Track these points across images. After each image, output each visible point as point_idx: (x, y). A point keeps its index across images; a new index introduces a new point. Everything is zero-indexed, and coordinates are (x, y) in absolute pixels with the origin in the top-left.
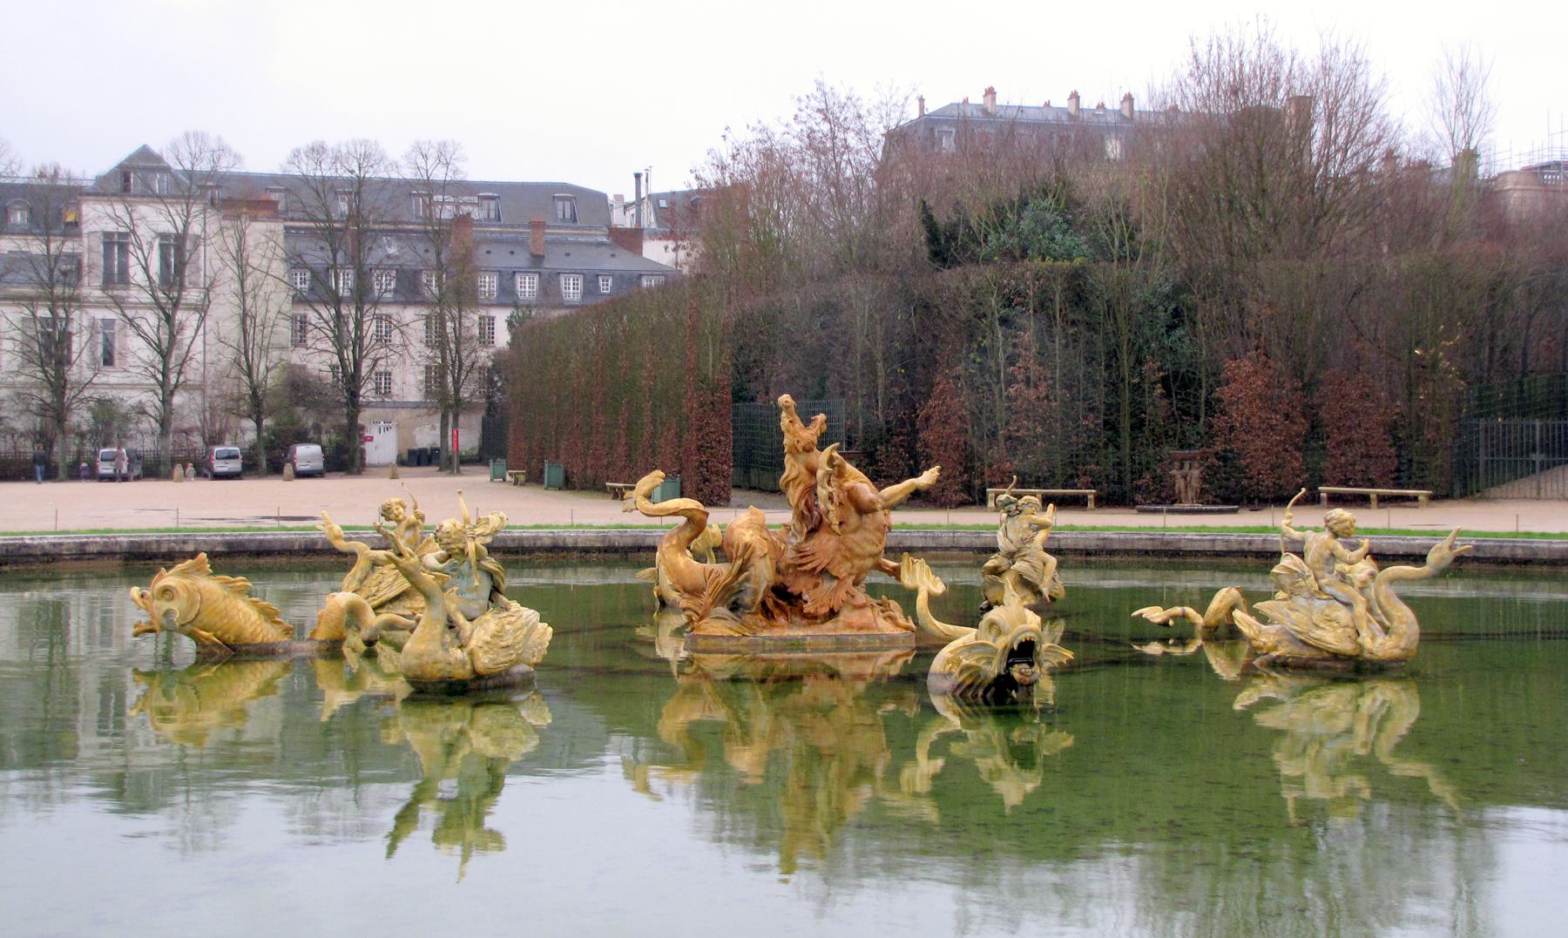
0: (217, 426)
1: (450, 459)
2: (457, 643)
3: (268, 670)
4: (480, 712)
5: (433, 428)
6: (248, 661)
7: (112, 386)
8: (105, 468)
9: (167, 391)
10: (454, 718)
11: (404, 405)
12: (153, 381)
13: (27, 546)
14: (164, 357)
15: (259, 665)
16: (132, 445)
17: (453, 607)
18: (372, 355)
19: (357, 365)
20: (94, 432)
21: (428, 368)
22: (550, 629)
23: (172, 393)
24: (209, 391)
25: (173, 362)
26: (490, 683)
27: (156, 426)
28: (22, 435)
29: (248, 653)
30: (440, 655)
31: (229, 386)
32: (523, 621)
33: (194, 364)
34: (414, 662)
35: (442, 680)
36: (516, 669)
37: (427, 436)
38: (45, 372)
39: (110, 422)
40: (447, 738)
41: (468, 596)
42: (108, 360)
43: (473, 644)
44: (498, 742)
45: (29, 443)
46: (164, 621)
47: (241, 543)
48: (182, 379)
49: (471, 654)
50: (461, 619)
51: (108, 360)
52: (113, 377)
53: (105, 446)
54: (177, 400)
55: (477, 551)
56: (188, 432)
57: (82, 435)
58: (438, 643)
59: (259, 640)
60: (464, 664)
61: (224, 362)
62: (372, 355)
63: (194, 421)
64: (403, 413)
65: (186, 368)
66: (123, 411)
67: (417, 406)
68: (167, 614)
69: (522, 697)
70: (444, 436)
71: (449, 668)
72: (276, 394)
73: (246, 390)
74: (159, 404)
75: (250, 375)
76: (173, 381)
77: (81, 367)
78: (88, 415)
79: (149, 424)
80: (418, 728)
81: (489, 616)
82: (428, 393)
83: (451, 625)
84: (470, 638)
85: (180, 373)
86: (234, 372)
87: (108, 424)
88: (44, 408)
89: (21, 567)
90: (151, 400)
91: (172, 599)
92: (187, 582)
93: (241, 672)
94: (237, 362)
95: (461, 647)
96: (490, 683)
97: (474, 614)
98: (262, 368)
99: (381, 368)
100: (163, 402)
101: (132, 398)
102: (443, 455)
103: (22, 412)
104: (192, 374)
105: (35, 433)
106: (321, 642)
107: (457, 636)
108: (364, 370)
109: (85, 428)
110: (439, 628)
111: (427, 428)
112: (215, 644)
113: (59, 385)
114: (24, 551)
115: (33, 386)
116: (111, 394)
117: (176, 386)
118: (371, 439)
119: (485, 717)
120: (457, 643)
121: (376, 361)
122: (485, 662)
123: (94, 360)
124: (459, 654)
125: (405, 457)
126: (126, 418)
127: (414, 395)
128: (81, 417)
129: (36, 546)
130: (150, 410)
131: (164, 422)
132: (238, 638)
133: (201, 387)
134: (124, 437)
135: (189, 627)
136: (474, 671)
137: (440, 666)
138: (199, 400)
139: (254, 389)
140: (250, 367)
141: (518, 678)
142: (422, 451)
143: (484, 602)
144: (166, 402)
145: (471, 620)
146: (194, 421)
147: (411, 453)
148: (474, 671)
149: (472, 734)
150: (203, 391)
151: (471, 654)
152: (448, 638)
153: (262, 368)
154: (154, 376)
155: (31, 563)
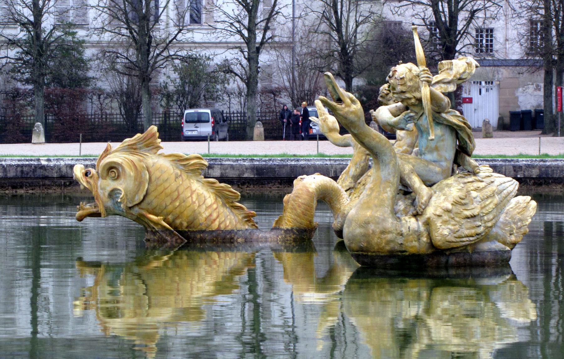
0: (307, 86)
1: (554, 122)
2: (412, 210)
3: (227, 261)
4: (439, 294)
5: (538, 88)
6: (202, 250)
7: (201, 44)
8: (189, 130)
9: (253, 51)
10: (406, 303)
11: (505, 63)
12: (238, 38)
13: (43, 167)
14: (249, 11)
15: (215, 255)
16: (219, 106)
17: (407, 168)
18: (469, 7)
19: (453, 18)
20: (181, 93)
21: (532, 22)
22: (534, 204)
23: (258, 50)
24: (298, 50)
25: (260, 16)
26: (452, 260)
27: (243, 85)
28: (108, 95)
29: (202, 241)
30: (390, 223)
31: (318, 41)
32: (493, 187)
33: (280, 18)
34: (358, 231)
35: (392, 254)
36: (486, 246)
37: (530, 98)
38: (129, 28)
39: (198, 82)
40: (401, 325)
41: (429, 157)
42: (196, 20)
43: (430, 212)
44: (462, 332)
45: (115, 104)
46: (109, 203)
47: (271, 169)
48: (269, 34)
49: (428, 223)
50: (416, 182)
51: (196, 20)
52: (198, 35)
53: (191, 107)
54: (264, 58)
55: (433, 98)
56: (275, 92)
57: (169, 97)
58: (388, 210)
59: (215, 226)
60: (419, 235)
61: (312, 16)
62: (469, 7)
63: (282, 80)
64: (504, 73)
65: (274, 24)
66: (210, 70)
67: (518, 63)
68: (113, 194)
69: (495, 281)
70: (547, 96)
71: (400, 240)
72: (367, 51)
73: (336, 46)
74: (245, 62)
75: (339, 30)
76: (259, 39)
77: (165, 26)
78: (175, 76)
79: (235, 84)
80: (364, 311)
81: (451, 180)
82: (532, 50)
83: (406, 190)
84: (427, 204)
85: (266, 29)
86: (324, 27)
87: (195, 85)
88: (130, 68)
89: (37, 191)
90: (236, 57)
91: (117, 178)
92: (134, 158)
93: (194, 265)
94: (325, 17)
95: (416, 215)
96: (452, 260)
97: (434, 179)
98: (352, 24)
99: (478, 22)
100: (249, 59)
101: (219, 56)
102: (547, 120)
103: (106, 71)
104: (281, 28)
105: (122, 94)
106: (287, 231)
107: (413, 203)
108: (460, 26)
109: (171, 88)
110: (389, 193)
111: (531, 89)
112: (165, 229)
113: (143, 42)
114: (39, 173)
115: (121, 44)
116: (194, 52)
117: (262, 43)
118: (470, 100)
119: (444, 301)
120: (412, 210)
121: (473, 13)
122: (444, 232)
123: (181, 17)
124: (412, 223)
125: (507, 120)
126: (212, 78)
127: (516, 52)
128: (168, 76)
129: (52, 168)
130: (237, 69)
131: (250, 81)
132: (190, 224)
133: (289, 46)
134: (211, 98)
135: (136, 211)
136: (431, 244)
137: (389, 236)
138: (288, 59)
139: (343, 44)
140: (339, 22)
141: (489, 258)
142: (527, 113)
143: (448, 164)
144: (252, 59)
145: (430, 184)
146: (282, 80)
147: (514, 115)
148: (431, 244)
149: (431, 322)
150: (293, 49)
151: (428, 223)
152: (401, 205)
153: (352, 24)
154: (239, 32)
155: (48, 187)
